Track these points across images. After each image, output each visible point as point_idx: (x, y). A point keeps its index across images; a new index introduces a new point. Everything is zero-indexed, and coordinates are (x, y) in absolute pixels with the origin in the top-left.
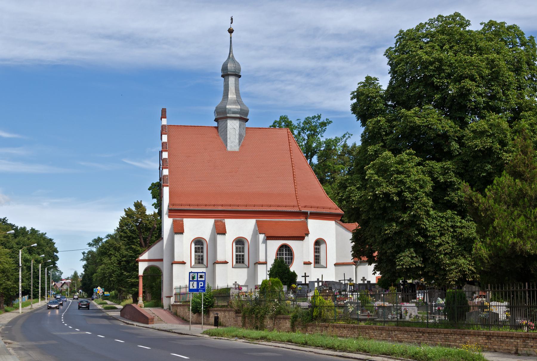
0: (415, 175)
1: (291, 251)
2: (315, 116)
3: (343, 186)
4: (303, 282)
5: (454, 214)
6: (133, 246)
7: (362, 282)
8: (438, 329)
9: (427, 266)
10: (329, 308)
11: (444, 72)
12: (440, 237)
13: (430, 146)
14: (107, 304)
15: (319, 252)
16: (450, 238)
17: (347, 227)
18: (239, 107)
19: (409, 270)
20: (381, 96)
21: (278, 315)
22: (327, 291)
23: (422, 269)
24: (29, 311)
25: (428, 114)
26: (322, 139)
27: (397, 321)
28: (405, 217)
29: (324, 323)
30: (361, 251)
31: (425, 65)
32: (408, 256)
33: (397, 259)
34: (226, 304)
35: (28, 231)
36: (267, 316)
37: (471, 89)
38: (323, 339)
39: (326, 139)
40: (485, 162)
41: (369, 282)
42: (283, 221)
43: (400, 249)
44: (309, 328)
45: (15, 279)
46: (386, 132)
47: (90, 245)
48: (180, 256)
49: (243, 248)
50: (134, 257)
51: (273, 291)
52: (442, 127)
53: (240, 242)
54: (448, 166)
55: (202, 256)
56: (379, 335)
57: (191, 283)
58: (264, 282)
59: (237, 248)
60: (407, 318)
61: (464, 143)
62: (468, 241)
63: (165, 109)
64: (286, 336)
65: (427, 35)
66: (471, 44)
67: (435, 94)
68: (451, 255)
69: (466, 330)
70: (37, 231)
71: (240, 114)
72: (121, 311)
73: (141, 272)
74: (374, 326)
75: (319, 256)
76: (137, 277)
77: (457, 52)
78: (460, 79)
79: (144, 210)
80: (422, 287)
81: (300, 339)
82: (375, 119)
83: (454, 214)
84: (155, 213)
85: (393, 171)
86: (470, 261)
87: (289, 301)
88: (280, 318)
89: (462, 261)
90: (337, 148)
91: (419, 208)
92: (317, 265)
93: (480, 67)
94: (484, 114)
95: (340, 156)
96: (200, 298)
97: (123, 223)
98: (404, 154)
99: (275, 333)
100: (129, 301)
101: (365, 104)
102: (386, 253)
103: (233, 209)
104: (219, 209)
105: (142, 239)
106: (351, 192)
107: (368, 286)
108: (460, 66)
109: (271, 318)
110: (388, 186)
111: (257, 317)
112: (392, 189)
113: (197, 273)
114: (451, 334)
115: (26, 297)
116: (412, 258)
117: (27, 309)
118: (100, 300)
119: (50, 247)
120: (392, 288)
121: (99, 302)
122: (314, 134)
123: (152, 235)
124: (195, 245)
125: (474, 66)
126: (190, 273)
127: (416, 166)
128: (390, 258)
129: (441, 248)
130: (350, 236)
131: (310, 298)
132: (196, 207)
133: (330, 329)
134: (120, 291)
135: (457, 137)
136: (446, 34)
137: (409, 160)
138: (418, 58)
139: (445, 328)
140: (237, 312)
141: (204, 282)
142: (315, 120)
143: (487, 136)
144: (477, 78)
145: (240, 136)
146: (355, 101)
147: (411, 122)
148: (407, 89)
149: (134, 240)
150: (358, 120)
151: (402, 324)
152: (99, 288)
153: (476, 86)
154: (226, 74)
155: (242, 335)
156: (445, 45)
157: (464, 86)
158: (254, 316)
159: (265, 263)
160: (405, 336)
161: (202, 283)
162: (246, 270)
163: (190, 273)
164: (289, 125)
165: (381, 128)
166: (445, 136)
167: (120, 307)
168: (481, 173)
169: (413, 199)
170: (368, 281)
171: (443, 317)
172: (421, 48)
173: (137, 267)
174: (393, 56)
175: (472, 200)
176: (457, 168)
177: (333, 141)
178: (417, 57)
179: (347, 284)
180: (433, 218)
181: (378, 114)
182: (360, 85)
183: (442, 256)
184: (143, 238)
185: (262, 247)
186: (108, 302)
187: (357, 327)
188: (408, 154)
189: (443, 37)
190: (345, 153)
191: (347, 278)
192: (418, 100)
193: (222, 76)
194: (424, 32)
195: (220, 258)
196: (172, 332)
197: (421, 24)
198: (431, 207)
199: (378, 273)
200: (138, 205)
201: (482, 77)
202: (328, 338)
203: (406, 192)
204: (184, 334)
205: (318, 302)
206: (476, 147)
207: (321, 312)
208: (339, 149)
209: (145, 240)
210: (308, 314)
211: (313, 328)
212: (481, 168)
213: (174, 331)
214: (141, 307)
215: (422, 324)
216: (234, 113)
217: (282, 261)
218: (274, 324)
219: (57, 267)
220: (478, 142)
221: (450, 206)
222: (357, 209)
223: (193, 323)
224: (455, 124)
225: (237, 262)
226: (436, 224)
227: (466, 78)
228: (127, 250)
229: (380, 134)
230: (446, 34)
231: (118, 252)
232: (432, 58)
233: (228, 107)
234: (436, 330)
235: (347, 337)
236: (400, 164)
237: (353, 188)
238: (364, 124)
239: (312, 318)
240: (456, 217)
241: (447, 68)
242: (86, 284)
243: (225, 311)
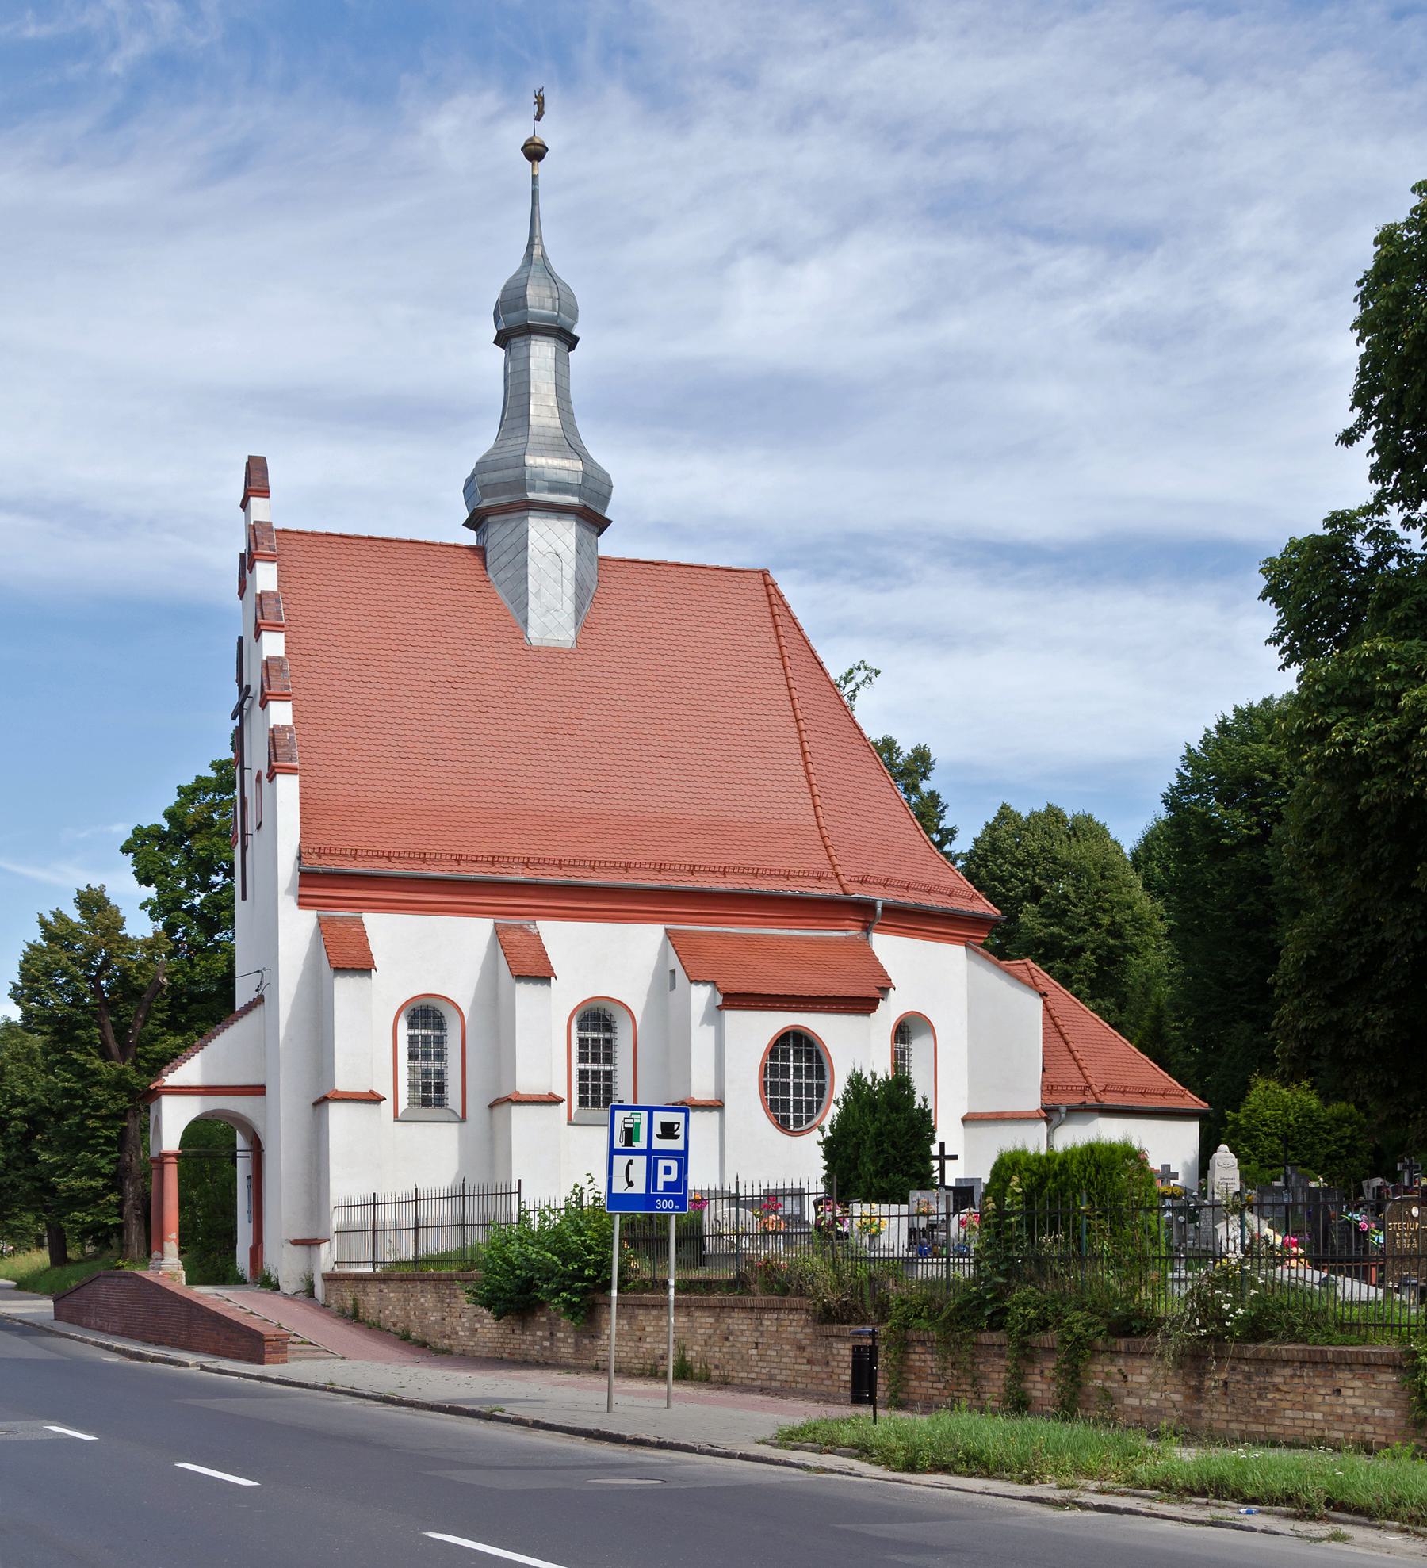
1: (819, 1060)
50: (81, 1097)
55: (440, 1073)
57: (620, 1161)
71: (580, 495)
103: (573, 880)
104: (515, 877)
105: (109, 1029)
123: (149, 1015)
132: (418, 865)
140: (827, 1316)
141: (682, 1156)
154: (514, 330)
161: (674, 1164)
185: (702, 1038)
195: (527, 1082)
200: (92, 902)
213: (512, 1411)
233: (530, 460)
243: (719, 1310)
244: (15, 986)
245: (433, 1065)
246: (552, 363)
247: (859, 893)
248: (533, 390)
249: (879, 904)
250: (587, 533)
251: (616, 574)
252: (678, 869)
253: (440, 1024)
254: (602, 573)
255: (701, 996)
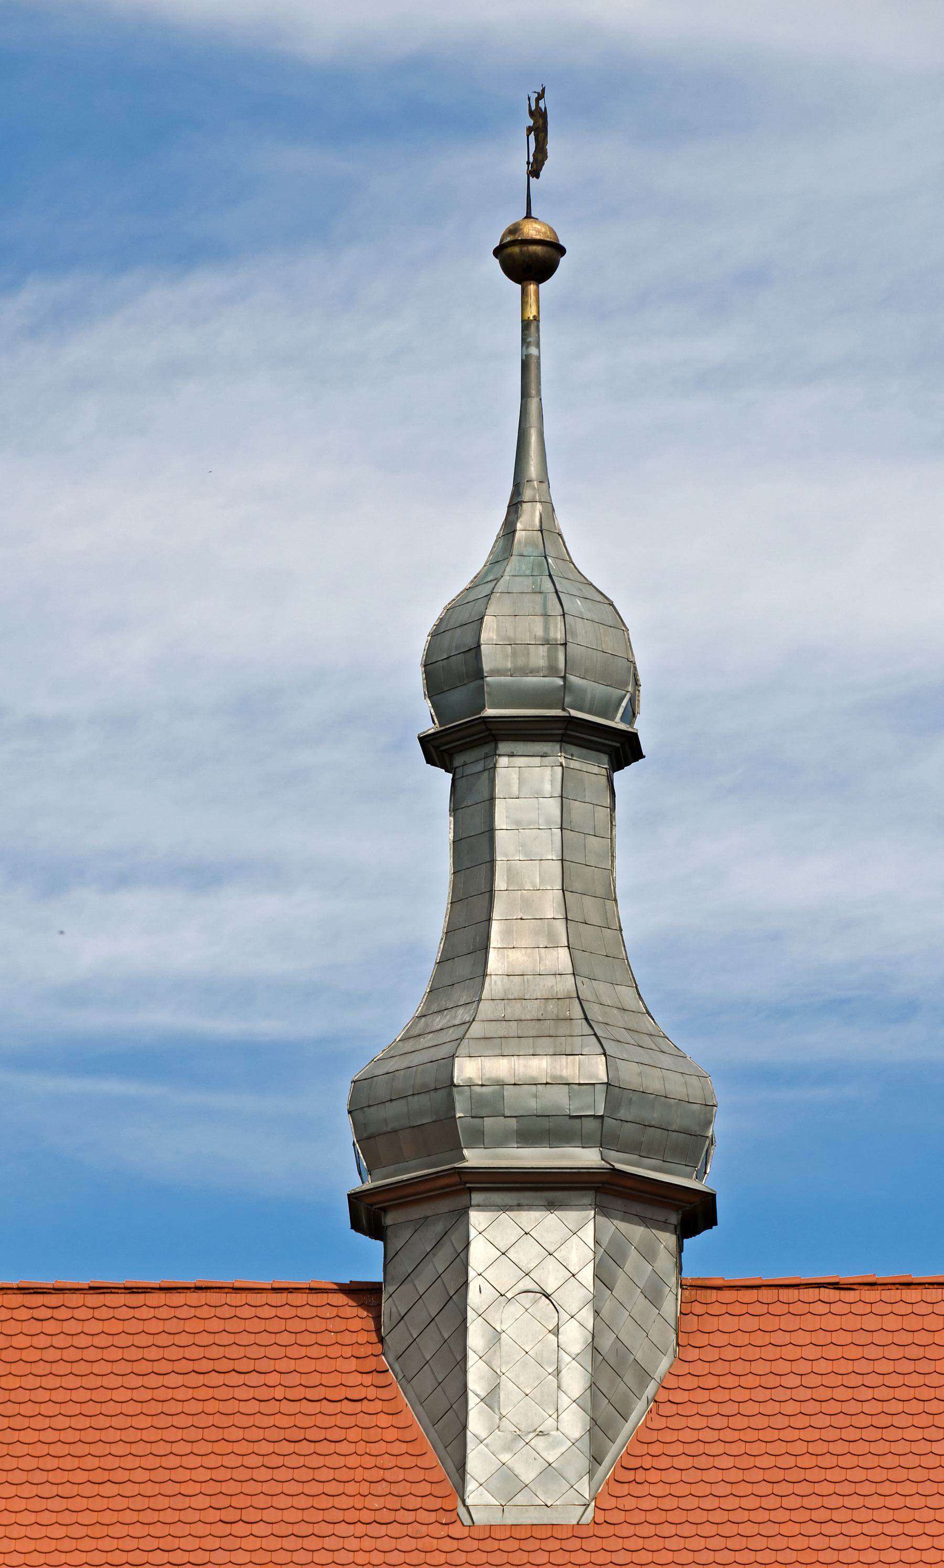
145: (607, 1364)
193: (436, 749)
233: (467, 1069)
248: (500, 883)
251: (729, 1323)
254: (691, 1323)
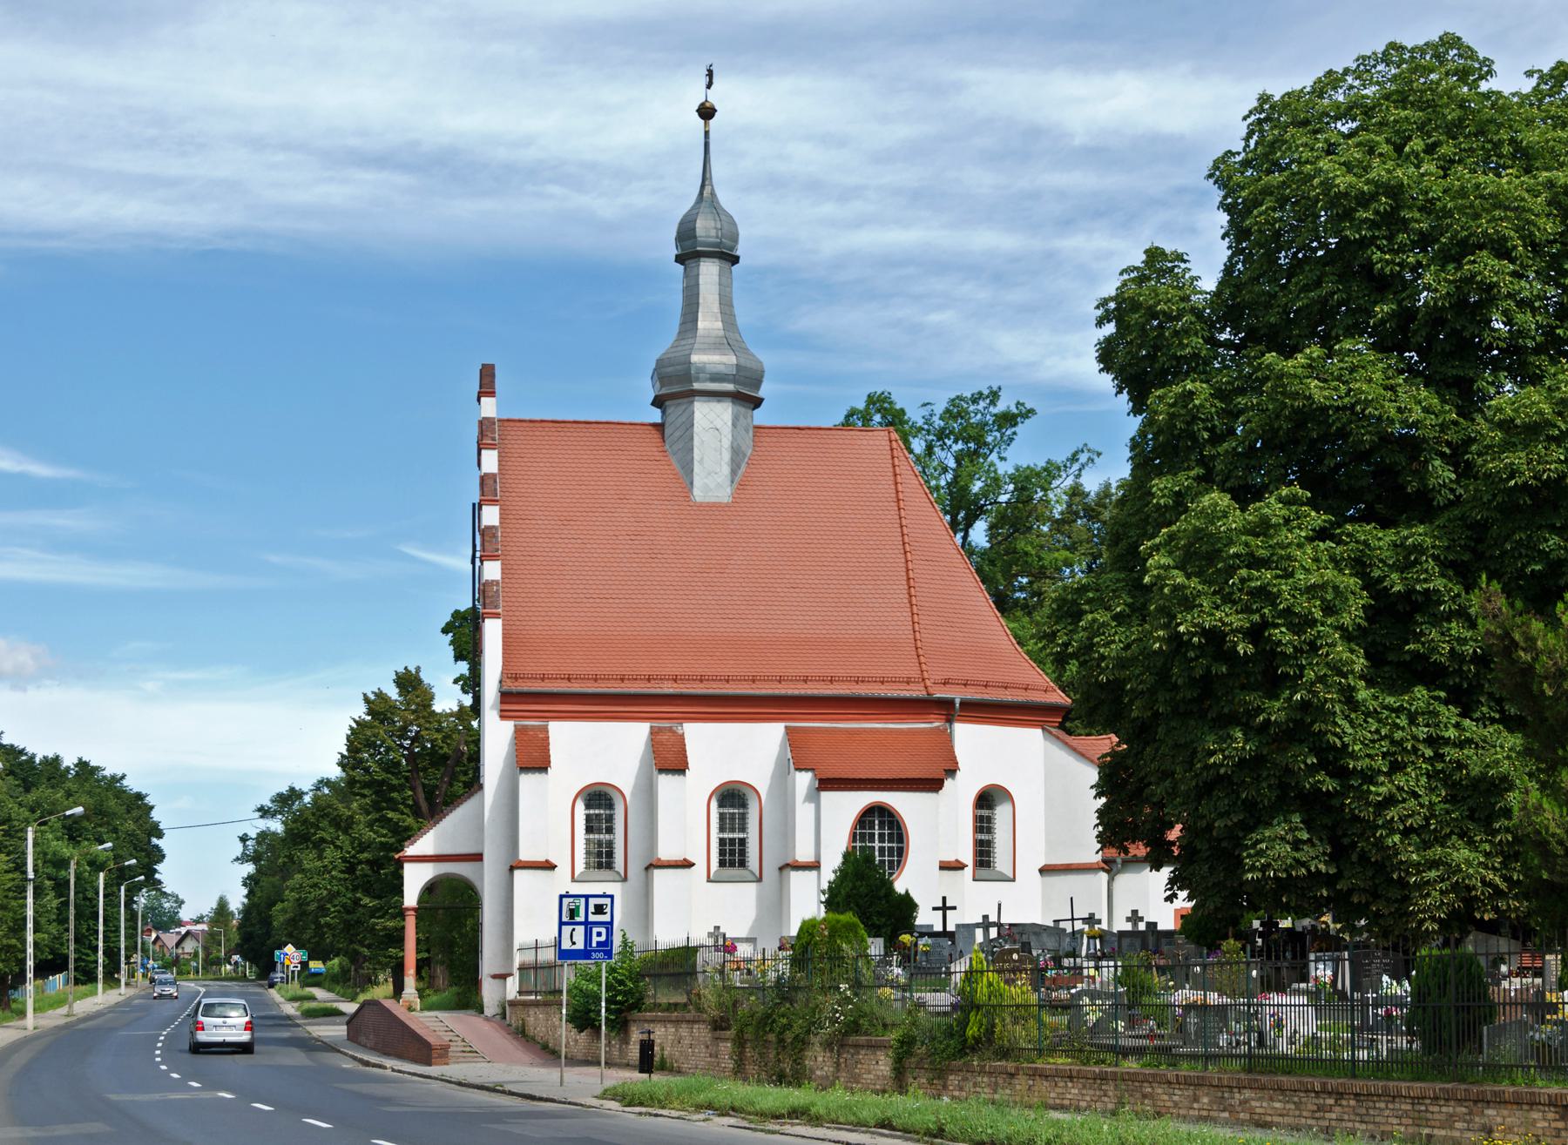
0: (1307, 571)
1: (899, 828)
2: (980, 393)
3: (1069, 610)
4: (938, 928)
5: (1437, 698)
6: (390, 815)
7: (1128, 927)
8: (1391, 1084)
9: (1346, 873)
10: (1021, 1012)
11: (1406, 231)
12: (1389, 774)
13: (1356, 473)
14: (313, 998)
15: (989, 830)
16: (1424, 780)
17: (1080, 748)
18: (732, 359)
19: (1283, 885)
20: (1194, 311)
21: (851, 1035)
22: (1015, 956)
23: (1329, 881)
24: (62, 1021)
25: (1353, 370)
26: (1004, 469)
27: (1250, 1056)
28: (1276, 710)
29: (1003, 1063)
30: (1127, 828)
31: (1344, 206)
32: (1282, 839)
33: (1247, 848)
34: (682, 999)
35: (68, 769)
36: (815, 1040)
37: (1496, 285)
38: (997, 1116)
39: (1017, 469)
40: (1539, 528)
41: (1152, 926)
42: (874, 730)
43: (1257, 817)
44: (953, 1080)
45: (15, 921)
46: (1212, 430)
47: (264, 812)
48: (530, 844)
49: (743, 817)
51: (836, 958)
52: (1400, 410)
53: (732, 798)
54: (1420, 539)
55: (610, 844)
56: (1186, 1104)
57: (567, 930)
58: (808, 928)
59: (722, 817)
60: (1283, 1047)
61: (1469, 465)
62: (1483, 787)
63: (492, 367)
64: (872, 1105)
65: (1351, 108)
66: (1496, 138)
67: (1376, 303)
68: (1424, 835)
69: (1489, 1088)
70: (97, 769)
72: (348, 1023)
73: (411, 898)
74: (1171, 1074)
75: (989, 843)
76: (401, 913)
77: (1452, 162)
78: (1464, 248)
79: (428, 697)
80: (1328, 944)
81: (918, 1117)
82: (1177, 389)
83: (1437, 698)
84: (461, 707)
85: (1237, 555)
86: (1487, 855)
87: (888, 990)
88: (857, 1046)
89: (1461, 854)
90: (1051, 495)
91: (1321, 679)
92: (983, 872)
93: (1524, 210)
94: (1539, 367)
95: (1058, 525)
96: (595, 978)
97: (359, 739)
98: (1272, 500)
99: (838, 1096)
100: (381, 992)
101: (1145, 338)
102: (1210, 827)
103: (711, 691)
105: (420, 790)
106: (1096, 629)
107: (1151, 940)
108: (1461, 209)
109: (828, 1045)
110: (1217, 608)
111: (781, 1041)
112: (1232, 619)
113: (587, 897)
114: (1436, 1098)
115: (58, 980)
116: (1297, 845)
117: (55, 1017)
118: (295, 988)
119: (136, 820)
120: (1230, 944)
121: (290, 994)
122: (976, 452)
123: (453, 777)
124: (588, 807)
125: (1507, 208)
126: (562, 897)
127: (1310, 539)
128: (1224, 844)
129: (1392, 813)
130: (1093, 775)
131: (957, 979)
133: (1021, 1083)
134: (355, 958)
135: (1449, 444)
136: (1412, 104)
137: (1287, 521)
138: (1322, 183)
139: (1413, 1080)
140: (718, 1025)
141: (609, 925)
142: (982, 404)
143: (1550, 439)
144: (1515, 247)
145: (736, 452)
146: (1110, 329)
147: (1295, 396)
148: (1283, 287)
149: (395, 795)
150: (1120, 392)
151: (1263, 1066)
152: (290, 949)
153: (1514, 274)
154: (689, 252)
155: (727, 1101)
156: (1410, 138)
157: (1473, 276)
158: (772, 1037)
159: (815, 866)
160: (1277, 1105)
161: (603, 930)
162: (751, 889)
163: (562, 897)
164: (895, 419)
165: (1195, 418)
166: (1412, 446)
167: (350, 1008)
168: (1529, 564)
169: (1302, 651)
170: (1149, 924)
171: (1402, 1042)
172: (1330, 150)
173: (399, 878)
174: (1237, 178)
175: (1513, 641)
176: (1448, 548)
177: (1038, 475)
178: (1316, 181)
179: (1081, 932)
180: (1368, 714)
181: (1187, 374)
182: (1126, 277)
183: (1397, 838)
184: (424, 785)
185: (804, 814)
186: (319, 993)
187: (1115, 1077)
188: (1288, 502)
189: (1403, 114)
190: (1076, 514)
191: (1082, 912)
192: (1322, 324)
193: (680, 259)
194: (1341, 98)
195: (665, 852)
196: (503, 1092)
197: (1330, 72)
198: (1362, 677)
199: (1183, 894)
200: (409, 682)
201: (1534, 245)
202: (1015, 1112)
203: (1276, 626)
204: (541, 1099)
205: (982, 991)
206: (1512, 477)
207: (994, 1026)
208: (1057, 498)
209: (430, 793)
210: (950, 1033)
211: (965, 1079)
212: (1528, 548)
213: (508, 1087)
214: (410, 1009)
215: (1333, 1066)
216: (716, 378)
217: (869, 859)
218: (838, 1064)
219: (160, 882)
220: (1517, 458)
221: (1425, 672)
222: (1116, 687)
223: (572, 1061)
224: (1444, 401)
225: (722, 864)
226: (1377, 731)
227: (1481, 247)
228: (370, 825)
229: (1193, 436)
230: (1412, 104)
231: (346, 832)
232: (1368, 182)
233: (695, 358)
234: (1385, 1088)
235: (1078, 1110)
236: (1257, 535)
237: (1102, 616)
238: (1138, 406)
239: (961, 1045)
240: (1442, 709)
241: (1417, 215)
242: (251, 939)
243: (677, 1022)
244: (343, 756)
245: (604, 837)
246: (716, 279)
247: (940, 693)
249: (958, 701)
250: (742, 410)
252: (795, 679)
253: (610, 805)
255: (804, 780)
